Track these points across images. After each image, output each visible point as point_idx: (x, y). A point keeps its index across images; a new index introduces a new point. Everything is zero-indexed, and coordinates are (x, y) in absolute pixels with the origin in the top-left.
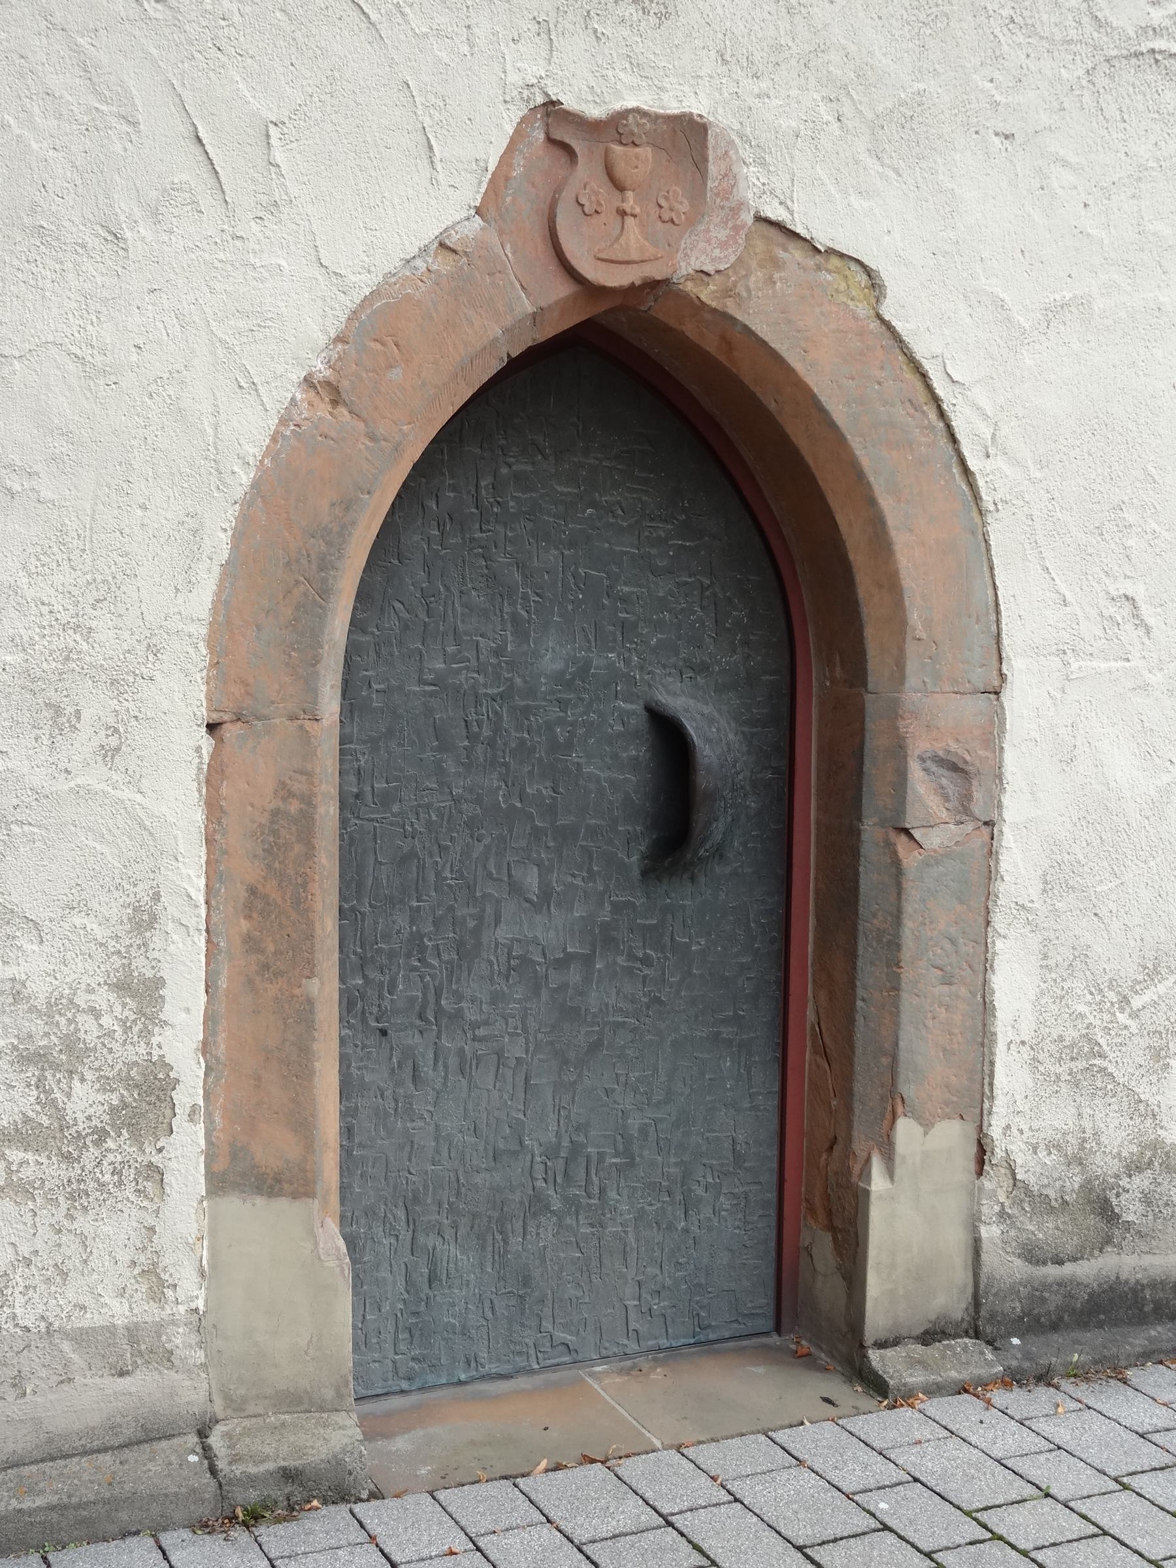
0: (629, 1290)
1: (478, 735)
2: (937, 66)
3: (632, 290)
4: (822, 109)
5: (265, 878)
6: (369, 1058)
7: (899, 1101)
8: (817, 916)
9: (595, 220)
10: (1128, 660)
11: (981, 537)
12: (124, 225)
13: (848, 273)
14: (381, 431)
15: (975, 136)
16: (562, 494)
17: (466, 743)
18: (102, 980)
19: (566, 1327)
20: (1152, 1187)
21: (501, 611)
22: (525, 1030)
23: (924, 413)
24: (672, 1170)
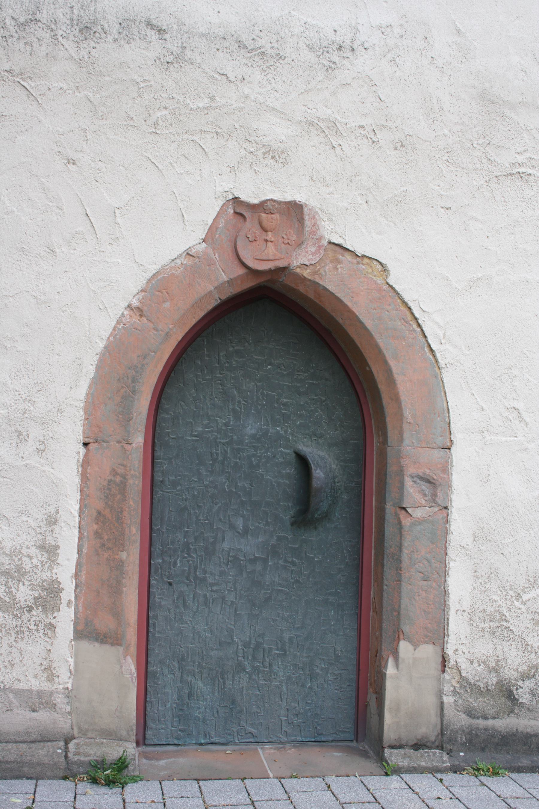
0: (283, 712)
1: (217, 459)
2: (412, 180)
3: (270, 271)
4: (359, 199)
5: (104, 508)
6: (163, 595)
7: (401, 633)
8: (375, 549)
9: (254, 244)
10: (516, 437)
11: (440, 379)
12: (56, 247)
13: (372, 265)
14: (160, 327)
15: (431, 208)
16: (256, 359)
17: (211, 462)
18: (33, 544)
19: (252, 725)
20: (535, 687)
21: (228, 407)
22: (235, 589)
23: (410, 324)
24: (305, 659)
